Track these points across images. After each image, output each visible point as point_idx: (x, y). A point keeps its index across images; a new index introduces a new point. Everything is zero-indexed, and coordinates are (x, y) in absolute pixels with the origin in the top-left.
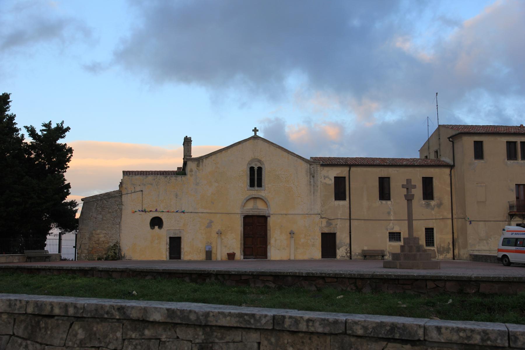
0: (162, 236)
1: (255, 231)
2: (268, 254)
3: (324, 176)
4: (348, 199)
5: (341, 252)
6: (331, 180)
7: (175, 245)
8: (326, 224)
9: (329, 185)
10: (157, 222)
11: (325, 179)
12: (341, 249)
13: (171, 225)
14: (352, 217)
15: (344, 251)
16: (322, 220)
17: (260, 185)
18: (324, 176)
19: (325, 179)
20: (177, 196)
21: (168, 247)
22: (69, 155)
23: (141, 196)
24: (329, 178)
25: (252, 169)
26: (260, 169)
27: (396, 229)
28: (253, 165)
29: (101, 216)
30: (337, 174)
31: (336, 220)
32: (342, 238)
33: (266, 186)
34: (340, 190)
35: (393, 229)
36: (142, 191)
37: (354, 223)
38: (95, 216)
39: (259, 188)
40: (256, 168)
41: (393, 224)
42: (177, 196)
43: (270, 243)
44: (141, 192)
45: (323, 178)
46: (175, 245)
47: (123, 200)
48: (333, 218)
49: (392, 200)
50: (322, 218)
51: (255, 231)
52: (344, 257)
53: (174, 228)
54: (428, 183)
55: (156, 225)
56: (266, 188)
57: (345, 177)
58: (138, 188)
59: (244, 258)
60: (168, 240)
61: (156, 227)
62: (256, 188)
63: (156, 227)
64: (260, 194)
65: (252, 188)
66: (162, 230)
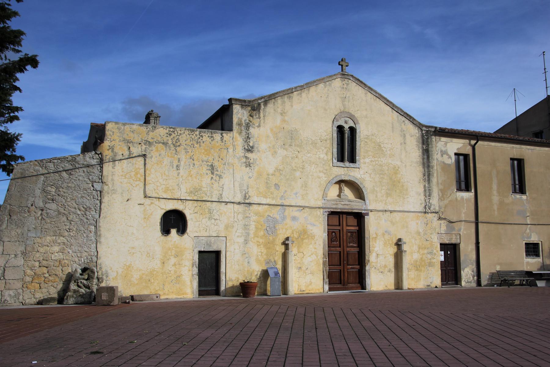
0: (185, 250)
1: (347, 238)
2: (368, 281)
3: (441, 151)
4: (473, 191)
5: (467, 274)
6: (450, 157)
7: (210, 264)
8: (445, 228)
9: (449, 165)
10: (174, 221)
11: (442, 156)
12: (466, 270)
13: (201, 229)
14: (480, 219)
15: (470, 272)
16: (440, 222)
17: (353, 159)
18: (441, 151)
19: (442, 156)
20: (212, 168)
21: (196, 270)
22: (435, 201)
23: (143, 167)
24: (448, 155)
25: (340, 129)
26: (353, 130)
27: (534, 239)
28: (341, 123)
29: (53, 206)
30: (458, 149)
31: (459, 223)
32: (467, 252)
33: (362, 161)
34: (466, 175)
35: (530, 237)
36: (144, 156)
37: (480, 226)
38: (41, 204)
39: (352, 165)
40: (346, 127)
41: (530, 229)
42: (212, 168)
43: (369, 261)
44: (141, 159)
45: (439, 154)
46: (210, 264)
47: (105, 173)
48: (454, 220)
49: (527, 194)
50: (440, 218)
51: (347, 238)
52: (471, 282)
53: (207, 234)
54: (518, 165)
55: (173, 228)
56: (362, 165)
57: (469, 155)
58: (136, 150)
59: (330, 289)
60: (196, 257)
61: (174, 231)
62: (347, 164)
63: (174, 231)
64: (352, 174)
65: (341, 164)
66: (185, 236)
